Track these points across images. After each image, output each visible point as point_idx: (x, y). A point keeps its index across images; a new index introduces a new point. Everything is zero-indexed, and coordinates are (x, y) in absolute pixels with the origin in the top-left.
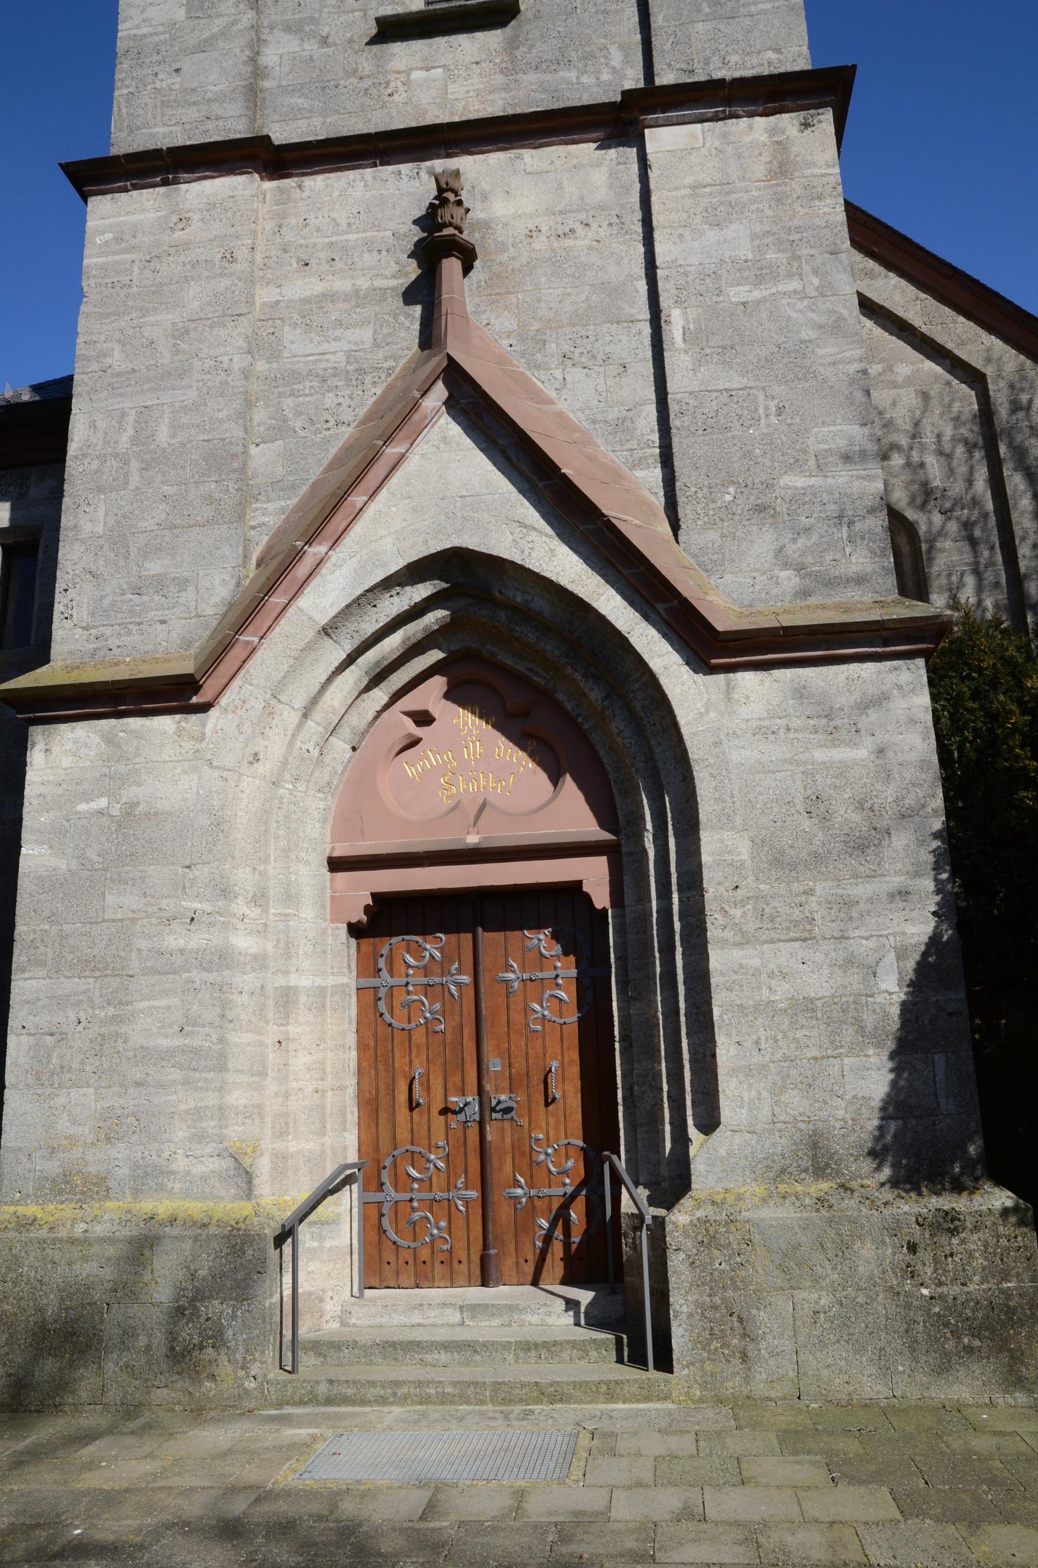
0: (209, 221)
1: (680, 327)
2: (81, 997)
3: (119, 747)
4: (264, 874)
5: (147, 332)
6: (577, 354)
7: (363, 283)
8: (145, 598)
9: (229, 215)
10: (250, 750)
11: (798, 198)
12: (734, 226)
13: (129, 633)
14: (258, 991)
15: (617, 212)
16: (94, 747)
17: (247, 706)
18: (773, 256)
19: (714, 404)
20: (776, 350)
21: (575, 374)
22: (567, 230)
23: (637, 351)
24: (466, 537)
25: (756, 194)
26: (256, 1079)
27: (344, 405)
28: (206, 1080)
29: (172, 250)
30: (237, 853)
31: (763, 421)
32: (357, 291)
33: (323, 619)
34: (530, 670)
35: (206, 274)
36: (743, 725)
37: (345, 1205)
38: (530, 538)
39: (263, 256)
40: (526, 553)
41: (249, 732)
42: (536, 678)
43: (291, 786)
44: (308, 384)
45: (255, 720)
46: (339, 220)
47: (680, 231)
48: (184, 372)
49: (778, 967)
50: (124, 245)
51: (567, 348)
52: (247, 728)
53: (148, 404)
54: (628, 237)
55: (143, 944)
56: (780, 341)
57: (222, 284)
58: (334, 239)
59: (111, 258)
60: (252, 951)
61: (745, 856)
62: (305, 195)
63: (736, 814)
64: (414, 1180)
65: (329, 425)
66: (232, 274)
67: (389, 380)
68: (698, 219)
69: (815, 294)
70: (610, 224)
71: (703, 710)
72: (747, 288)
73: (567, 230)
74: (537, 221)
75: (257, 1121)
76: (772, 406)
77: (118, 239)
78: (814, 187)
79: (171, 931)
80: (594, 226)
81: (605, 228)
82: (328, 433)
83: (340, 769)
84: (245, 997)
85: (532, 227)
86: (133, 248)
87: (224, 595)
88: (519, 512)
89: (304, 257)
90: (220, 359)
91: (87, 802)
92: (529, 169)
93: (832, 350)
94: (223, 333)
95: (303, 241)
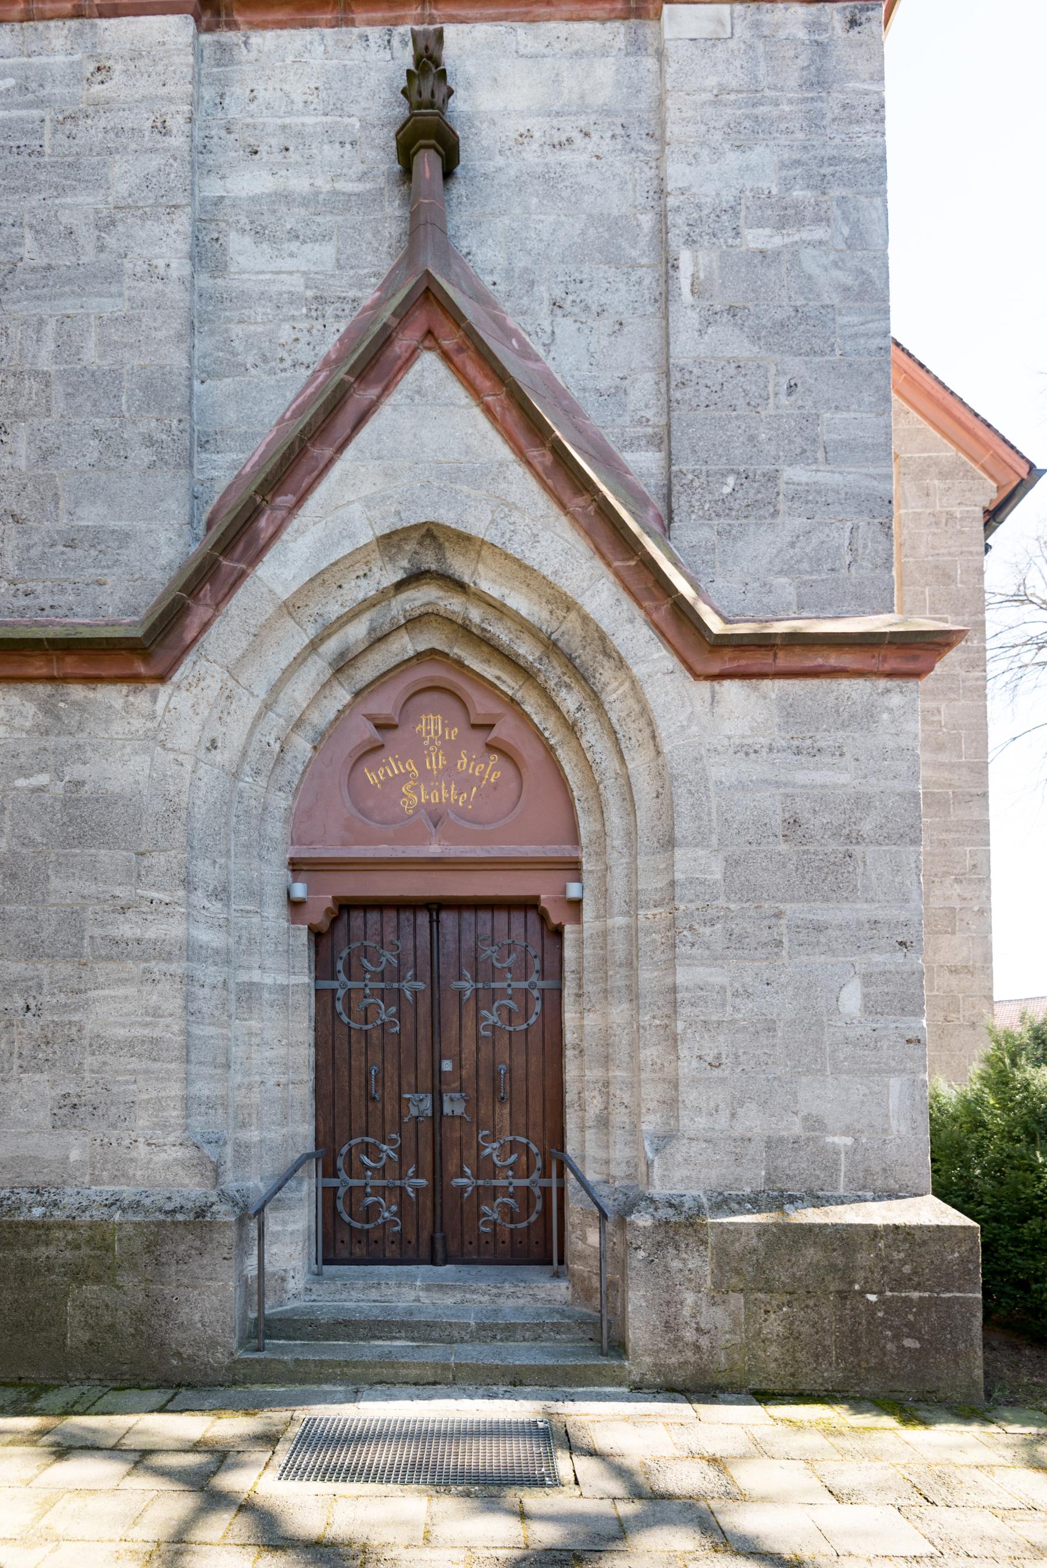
0: (135, 74)
1: (689, 274)
2: (30, 983)
3: (58, 718)
4: (225, 867)
5: (66, 218)
6: (568, 302)
7: (323, 184)
8: (80, 552)
9: (160, 68)
10: (208, 735)
11: (834, 120)
12: (759, 149)
13: (63, 591)
14: (220, 985)
15: (622, 120)
16: (30, 717)
17: (202, 684)
18: (801, 193)
19: (719, 375)
20: (793, 314)
21: (566, 327)
22: (563, 139)
23: (636, 305)
24: (442, 511)
25: (787, 108)
26: (219, 1071)
27: (303, 341)
28: (167, 1071)
29: (91, 110)
30: (195, 843)
31: (771, 400)
32: (317, 194)
33: (284, 594)
34: (498, 678)
35: (133, 146)
36: (726, 742)
37: (306, 1189)
38: (512, 520)
39: (202, 134)
40: (507, 536)
41: (206, 713)
42: (503, 687)
43: (250, 780)
44: (260, 310)
45: (212, 701)
46: (293, 96)
47: (696, 149)
48: (114, 275)
49: (743, 986)
50: (30, 97)
51: (558, 292)
52: (204, 710)
53: (70, 312)
54: (633, 155)
55: (97, 932)
56: (799, 303)
57: (154, 163)
58: (287, 121)
59: (15, 113)
60: (214, 945)
61: (718, 876)
62: (253, 55)
63: (711, 833)
64: (368, 1168)
65: (285, 365)
66: (166, 150)
67: (355, 314)
68: (718, 136)
69: (843, 246)
70: (613, 136)
71: (685, 723)
72: (768, 231)
73: (563, 139)
74: (530, 123)
75: (220, 1111)
76: (784, 381)
77: (24, 89)
78: (853, 107)
79: (127, 920)
80: (595, 137)
81: (608, 140)
82: (283, 374)
83: (300, 768)
84: (207, 990)
85: (523, 130)
86: (40, 103)
87: (171, 557)
88: (501, 487)
89: (252, 141)
90: (154, 262)
91: (26, 776)
92: (522, 51)
93: (855, 319)
94: (157, 230)
95: (249, 120)
